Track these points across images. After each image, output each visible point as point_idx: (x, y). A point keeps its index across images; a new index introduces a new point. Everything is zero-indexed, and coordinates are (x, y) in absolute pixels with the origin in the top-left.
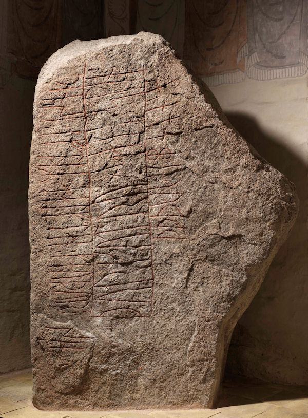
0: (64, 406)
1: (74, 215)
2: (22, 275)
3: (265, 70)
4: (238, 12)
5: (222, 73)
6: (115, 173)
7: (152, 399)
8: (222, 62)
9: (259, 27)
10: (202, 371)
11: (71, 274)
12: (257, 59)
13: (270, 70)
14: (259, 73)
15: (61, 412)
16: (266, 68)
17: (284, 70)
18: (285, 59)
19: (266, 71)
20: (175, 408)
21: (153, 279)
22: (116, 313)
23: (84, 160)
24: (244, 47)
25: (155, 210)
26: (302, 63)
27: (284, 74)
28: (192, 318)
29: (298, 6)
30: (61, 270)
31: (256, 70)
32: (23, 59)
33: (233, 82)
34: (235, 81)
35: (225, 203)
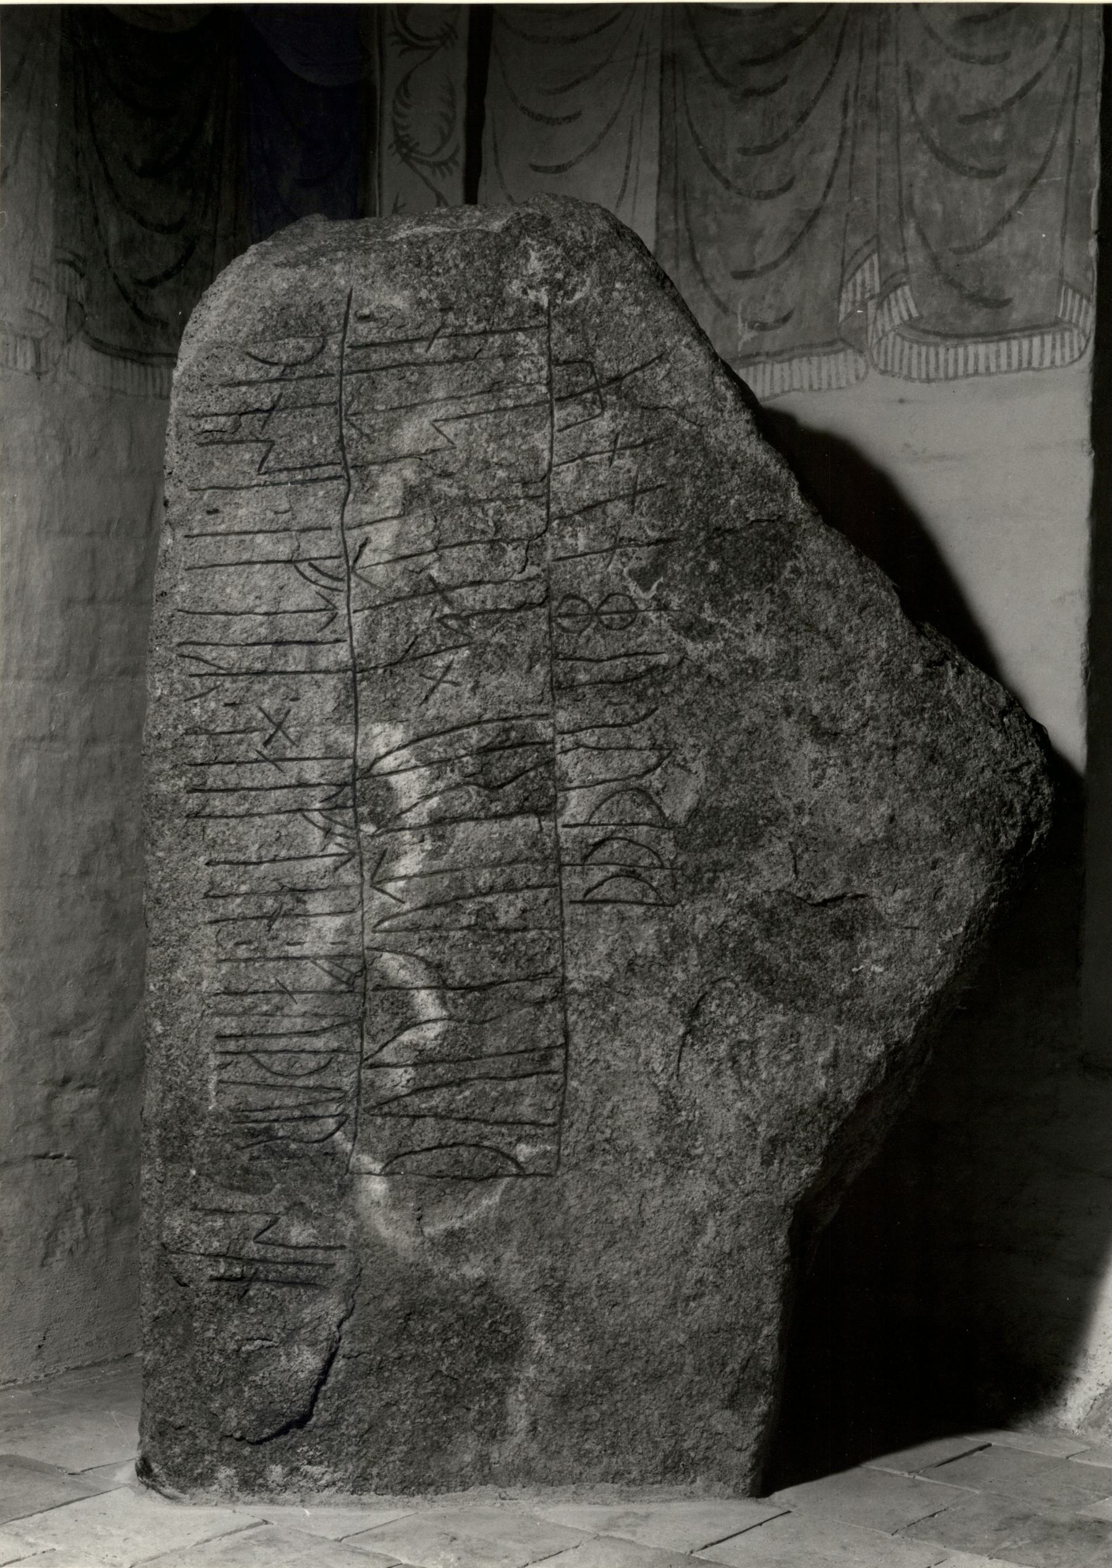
0: (251, 1483)
1: (299, 815)
2: (90, 1034)
3: (936, 345)
4: (848, 143)
5: (786, 356)
6: (445, 674)
7: (554, 1465)
8: (786, 319)
9: (917, 201)
10: (728, 1369)
11: (286, 1024)
12: (908, 310)
13: (956, 347)
14: (915, 356)
15: (240, 1508)
16: (938, 339)
17: (1003, 345)
18: (1006, 308)
19: (942, 350)
20: (635, 1494)
21: (565, 1045)
22: (442, 1161)
23: (341, 625)
24: (866, 265)
25: (578, 805)
26: (1070, 322)
27: (1003, 361)
28: (697, 1189)
29: (1058, 124)
30: (246, 1012)
31: (907, 345)
33: (825, 386)
34: (829, 384)
35: (816, 786)
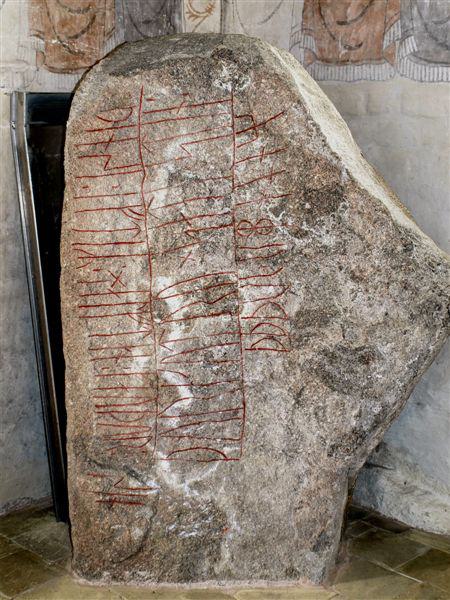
8: (360, 45)
19: (427, 68)
23: (142, 235)
24: (395, 25)
32: (54, 42)
